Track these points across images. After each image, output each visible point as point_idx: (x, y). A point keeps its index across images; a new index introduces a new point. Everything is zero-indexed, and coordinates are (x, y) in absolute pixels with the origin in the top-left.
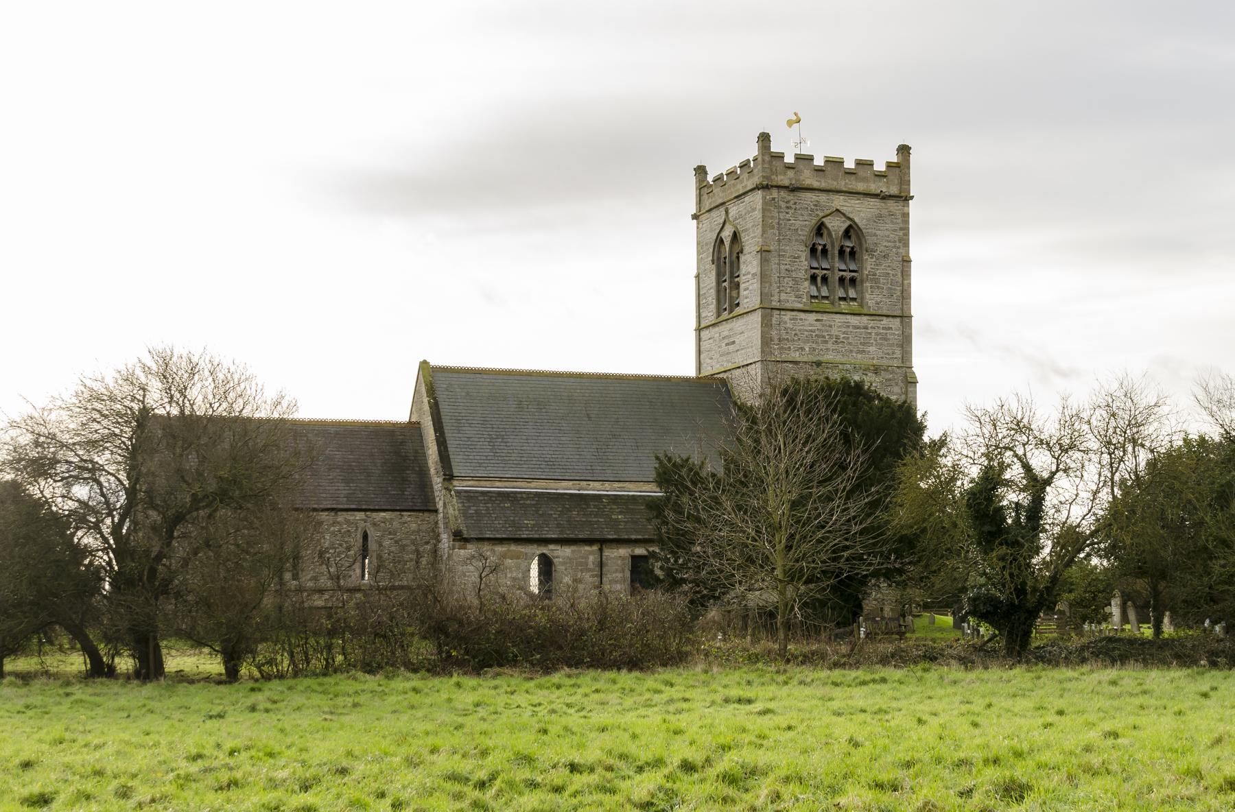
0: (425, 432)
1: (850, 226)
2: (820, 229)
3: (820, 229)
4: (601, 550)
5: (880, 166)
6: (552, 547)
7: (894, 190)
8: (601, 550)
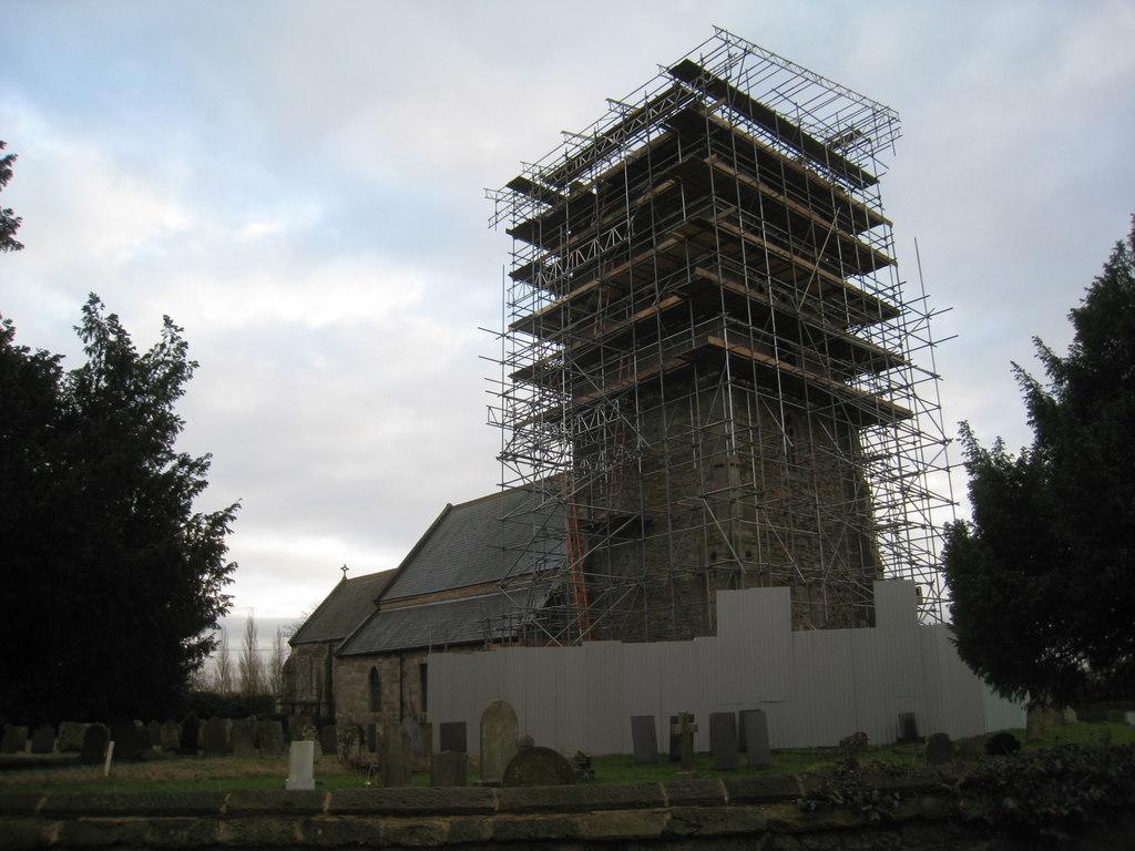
4: (402, 660)
8: (402, 660)
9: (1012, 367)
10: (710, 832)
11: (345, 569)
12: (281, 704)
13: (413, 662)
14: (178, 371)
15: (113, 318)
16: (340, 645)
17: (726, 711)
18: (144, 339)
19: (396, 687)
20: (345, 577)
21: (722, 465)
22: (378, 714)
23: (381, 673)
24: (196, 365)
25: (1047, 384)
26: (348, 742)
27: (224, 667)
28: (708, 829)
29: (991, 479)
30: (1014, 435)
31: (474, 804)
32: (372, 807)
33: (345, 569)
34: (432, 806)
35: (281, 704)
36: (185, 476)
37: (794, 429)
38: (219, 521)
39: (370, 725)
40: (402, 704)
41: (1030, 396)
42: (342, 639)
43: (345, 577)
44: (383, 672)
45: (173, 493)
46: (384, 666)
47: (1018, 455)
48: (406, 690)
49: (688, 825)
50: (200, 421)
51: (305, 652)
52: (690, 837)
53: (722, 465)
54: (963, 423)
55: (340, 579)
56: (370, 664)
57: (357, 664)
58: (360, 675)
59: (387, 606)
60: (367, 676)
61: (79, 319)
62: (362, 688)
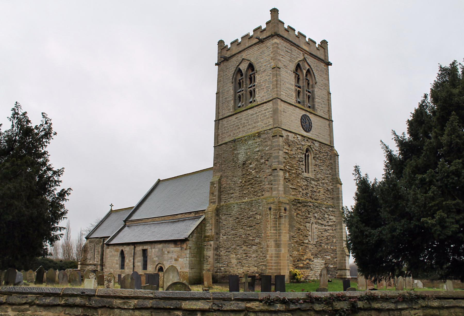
4: (135, 247)
6: (125, 247)
8: (135, 247)
9: (380, 143)
10: (225, 309)
11: (112, 205)
12: (81, 264)
13: (139, 249)
14: (48, 134)
15: (24, 114)
16: (108, 240)
17: (342, 284)
18: (35, 121)
19: (132, 259)
20: (111, 209)
21: (276, 169)
22: (123, 270)
23: (125, 252)
24: (55, 134)
25: (396, 151)
26: (109, 281)
27: (67, 248)
28: (225, 308)
29: (364, 187)
30: (377, 173)
31: (146, 295)
32: (112, 295)
33: (112, 205)
34: (132, 296)
35: (81, 264)
36: (51, 177)
37: (310, 154)
38: (63, 194)
39: (119, 275)
40: (134, 266)
41: (388, 155)
42: (109, 237)
43: (111, 209)
44: (126, 252)
45: (45, 184)
46: (127, 249)
47: (373, 182)
48: (136, 261)
49: (218, 306)
50: (55, 154)
51: (90, 242)
52: (218, 310)
53: (276, 169)
54: (356, 167)
55: (109, 210)
56: (120, 248)
57: (115, 248)
58: (116, 253)
59: (130, 223)
60: (119, 253)
61: (10, 114)
62: (117, 258)
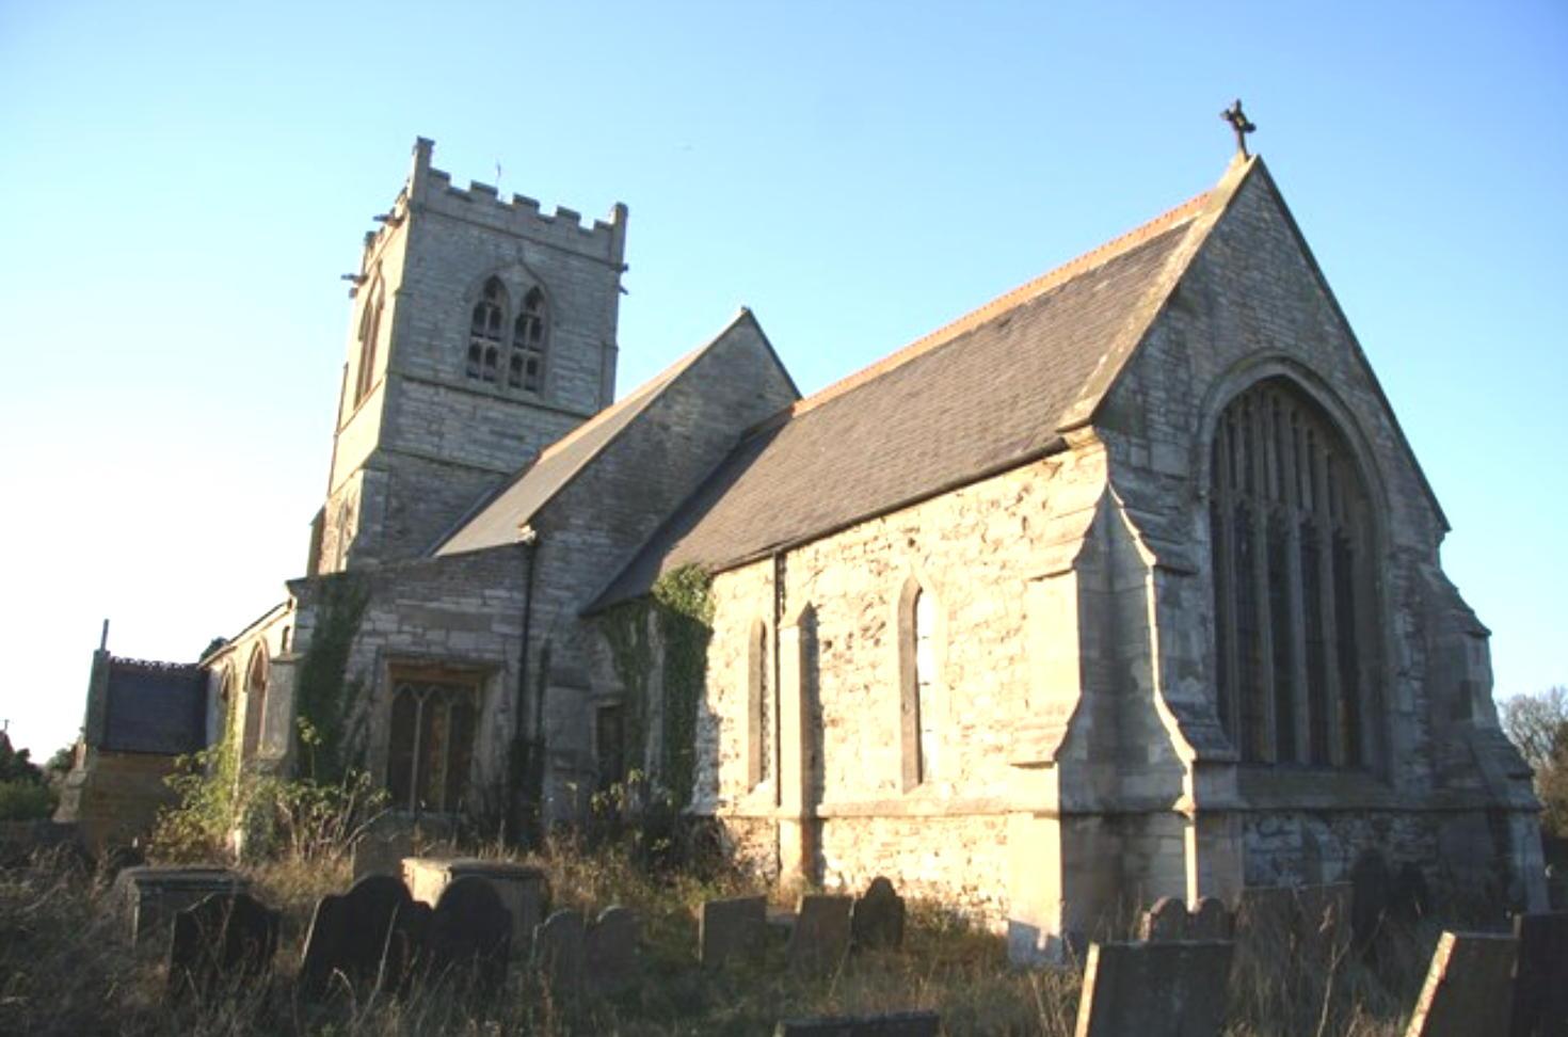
0: (1290, 380)
1: (536, 289)
2: (493, 286)
3: (493, 286)
5: (587, 223)
7: (600, 253)
